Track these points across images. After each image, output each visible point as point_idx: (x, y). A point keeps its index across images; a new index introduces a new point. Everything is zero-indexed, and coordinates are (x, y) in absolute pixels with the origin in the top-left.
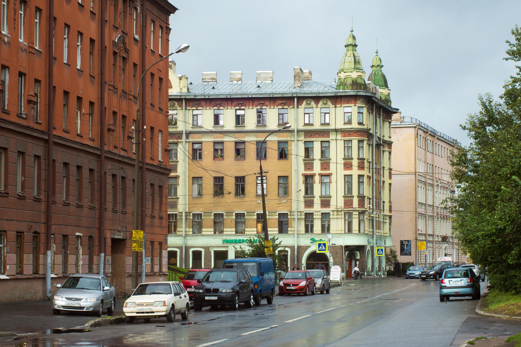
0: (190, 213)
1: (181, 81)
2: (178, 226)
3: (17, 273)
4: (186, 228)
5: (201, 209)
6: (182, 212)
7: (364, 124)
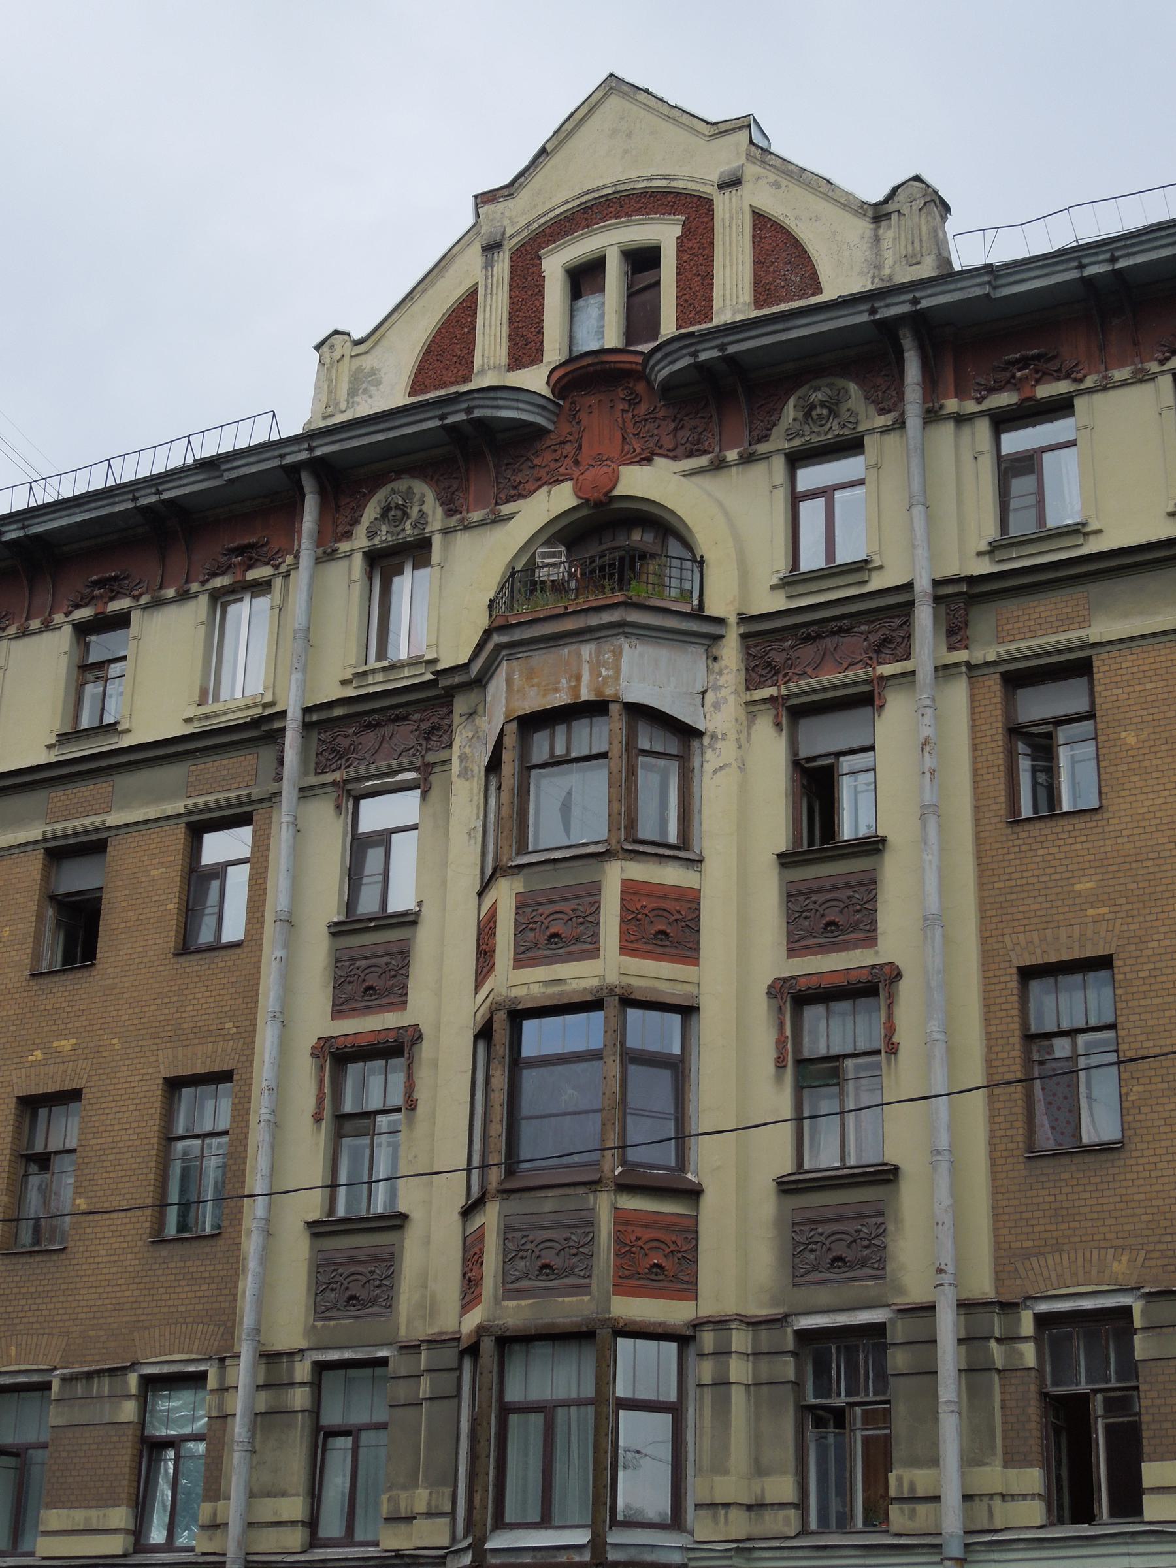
0: (1008, 1307)
1: (888, 234)
2: (899, 1452)
4: (971, 1460)
5: (1120, 1267)
6: (931, 1308)
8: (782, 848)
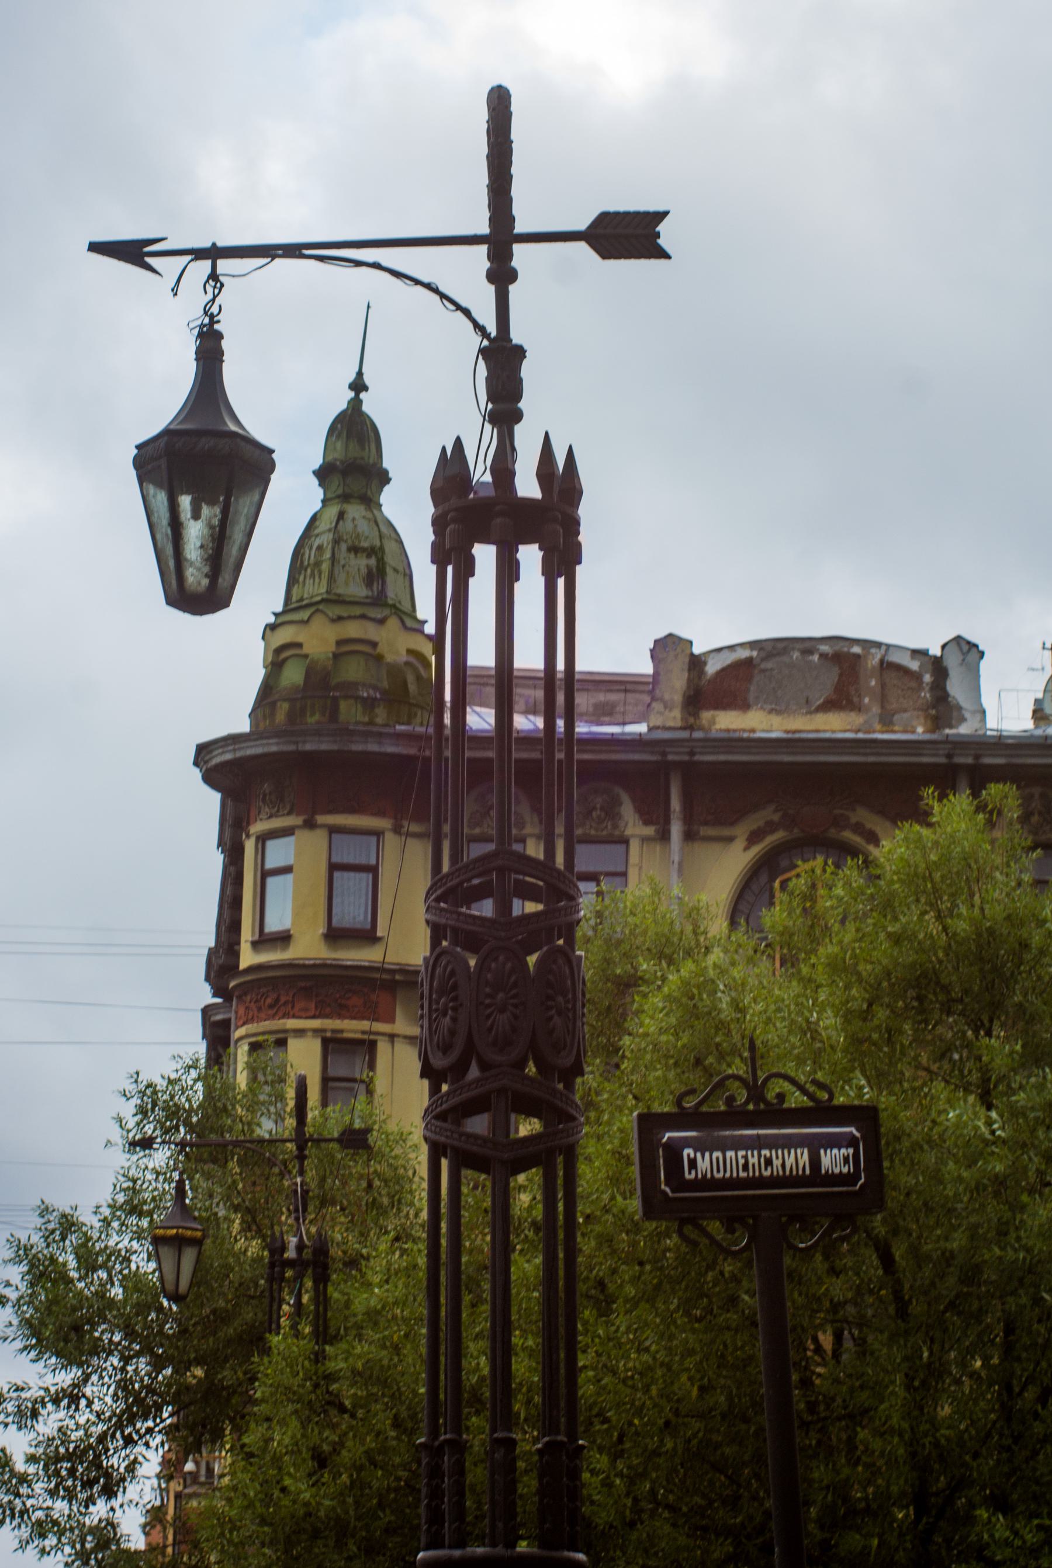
3: (367, 1047)
7: (379, 934)
8: (317, 461)
